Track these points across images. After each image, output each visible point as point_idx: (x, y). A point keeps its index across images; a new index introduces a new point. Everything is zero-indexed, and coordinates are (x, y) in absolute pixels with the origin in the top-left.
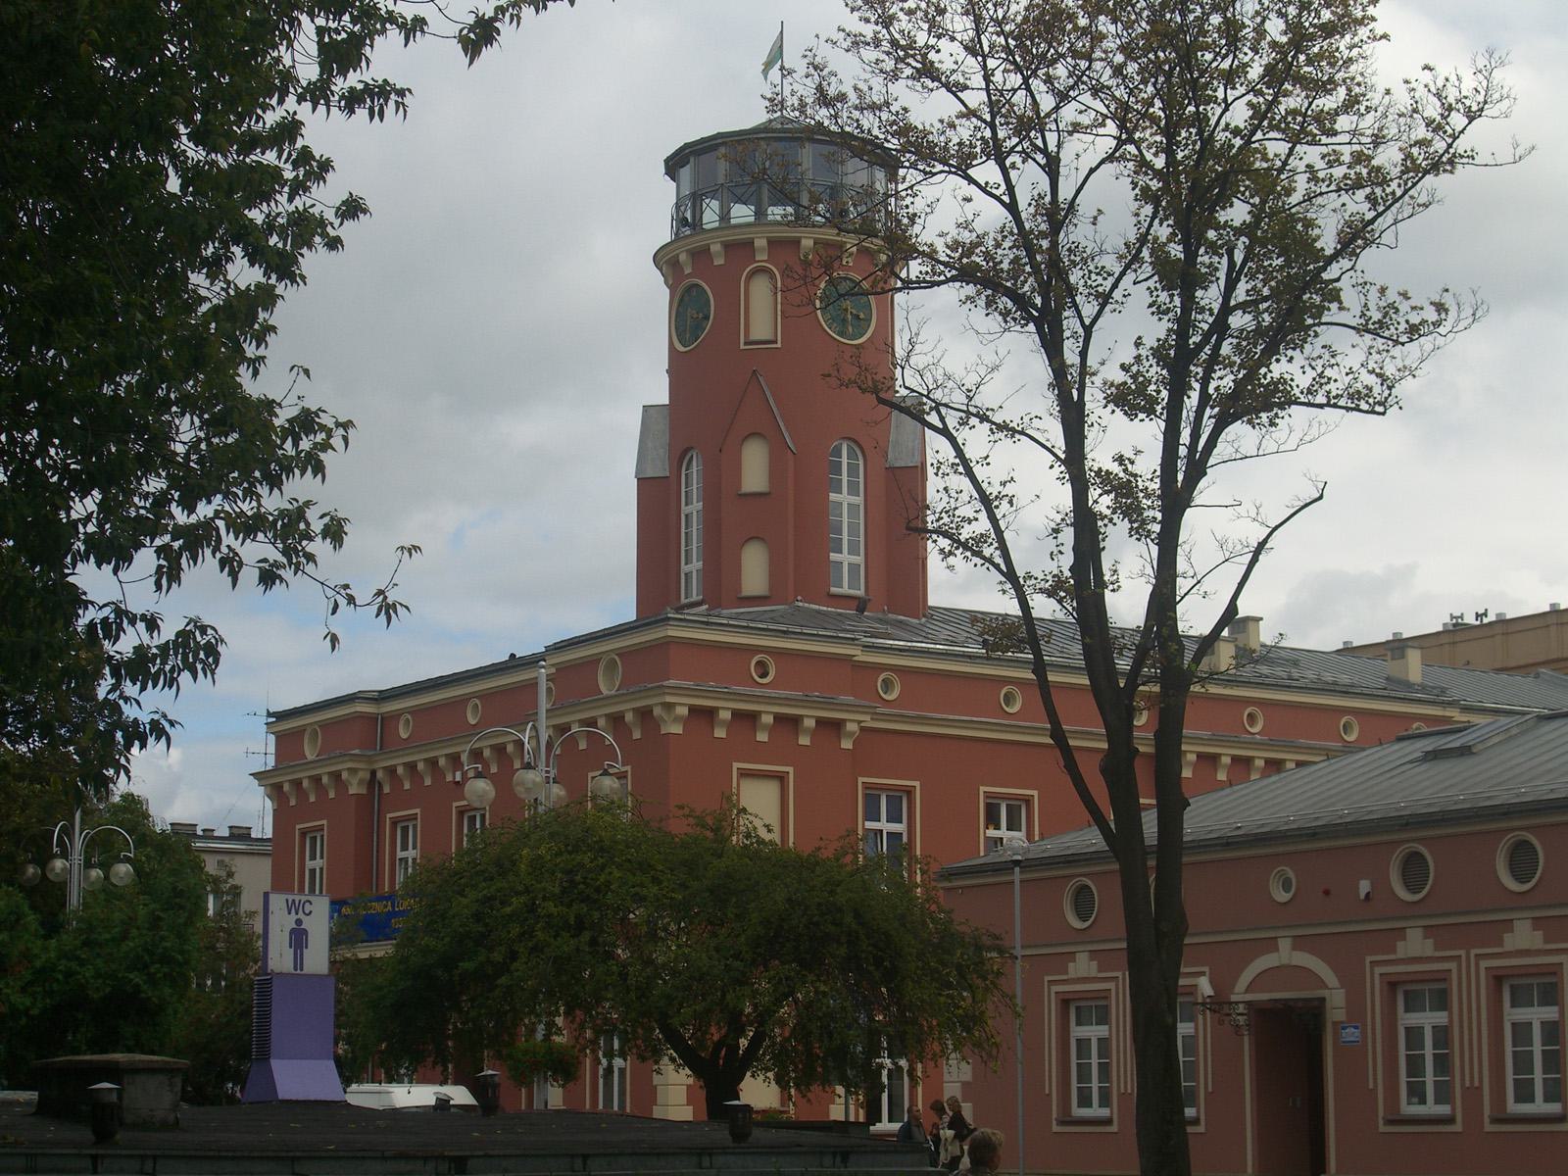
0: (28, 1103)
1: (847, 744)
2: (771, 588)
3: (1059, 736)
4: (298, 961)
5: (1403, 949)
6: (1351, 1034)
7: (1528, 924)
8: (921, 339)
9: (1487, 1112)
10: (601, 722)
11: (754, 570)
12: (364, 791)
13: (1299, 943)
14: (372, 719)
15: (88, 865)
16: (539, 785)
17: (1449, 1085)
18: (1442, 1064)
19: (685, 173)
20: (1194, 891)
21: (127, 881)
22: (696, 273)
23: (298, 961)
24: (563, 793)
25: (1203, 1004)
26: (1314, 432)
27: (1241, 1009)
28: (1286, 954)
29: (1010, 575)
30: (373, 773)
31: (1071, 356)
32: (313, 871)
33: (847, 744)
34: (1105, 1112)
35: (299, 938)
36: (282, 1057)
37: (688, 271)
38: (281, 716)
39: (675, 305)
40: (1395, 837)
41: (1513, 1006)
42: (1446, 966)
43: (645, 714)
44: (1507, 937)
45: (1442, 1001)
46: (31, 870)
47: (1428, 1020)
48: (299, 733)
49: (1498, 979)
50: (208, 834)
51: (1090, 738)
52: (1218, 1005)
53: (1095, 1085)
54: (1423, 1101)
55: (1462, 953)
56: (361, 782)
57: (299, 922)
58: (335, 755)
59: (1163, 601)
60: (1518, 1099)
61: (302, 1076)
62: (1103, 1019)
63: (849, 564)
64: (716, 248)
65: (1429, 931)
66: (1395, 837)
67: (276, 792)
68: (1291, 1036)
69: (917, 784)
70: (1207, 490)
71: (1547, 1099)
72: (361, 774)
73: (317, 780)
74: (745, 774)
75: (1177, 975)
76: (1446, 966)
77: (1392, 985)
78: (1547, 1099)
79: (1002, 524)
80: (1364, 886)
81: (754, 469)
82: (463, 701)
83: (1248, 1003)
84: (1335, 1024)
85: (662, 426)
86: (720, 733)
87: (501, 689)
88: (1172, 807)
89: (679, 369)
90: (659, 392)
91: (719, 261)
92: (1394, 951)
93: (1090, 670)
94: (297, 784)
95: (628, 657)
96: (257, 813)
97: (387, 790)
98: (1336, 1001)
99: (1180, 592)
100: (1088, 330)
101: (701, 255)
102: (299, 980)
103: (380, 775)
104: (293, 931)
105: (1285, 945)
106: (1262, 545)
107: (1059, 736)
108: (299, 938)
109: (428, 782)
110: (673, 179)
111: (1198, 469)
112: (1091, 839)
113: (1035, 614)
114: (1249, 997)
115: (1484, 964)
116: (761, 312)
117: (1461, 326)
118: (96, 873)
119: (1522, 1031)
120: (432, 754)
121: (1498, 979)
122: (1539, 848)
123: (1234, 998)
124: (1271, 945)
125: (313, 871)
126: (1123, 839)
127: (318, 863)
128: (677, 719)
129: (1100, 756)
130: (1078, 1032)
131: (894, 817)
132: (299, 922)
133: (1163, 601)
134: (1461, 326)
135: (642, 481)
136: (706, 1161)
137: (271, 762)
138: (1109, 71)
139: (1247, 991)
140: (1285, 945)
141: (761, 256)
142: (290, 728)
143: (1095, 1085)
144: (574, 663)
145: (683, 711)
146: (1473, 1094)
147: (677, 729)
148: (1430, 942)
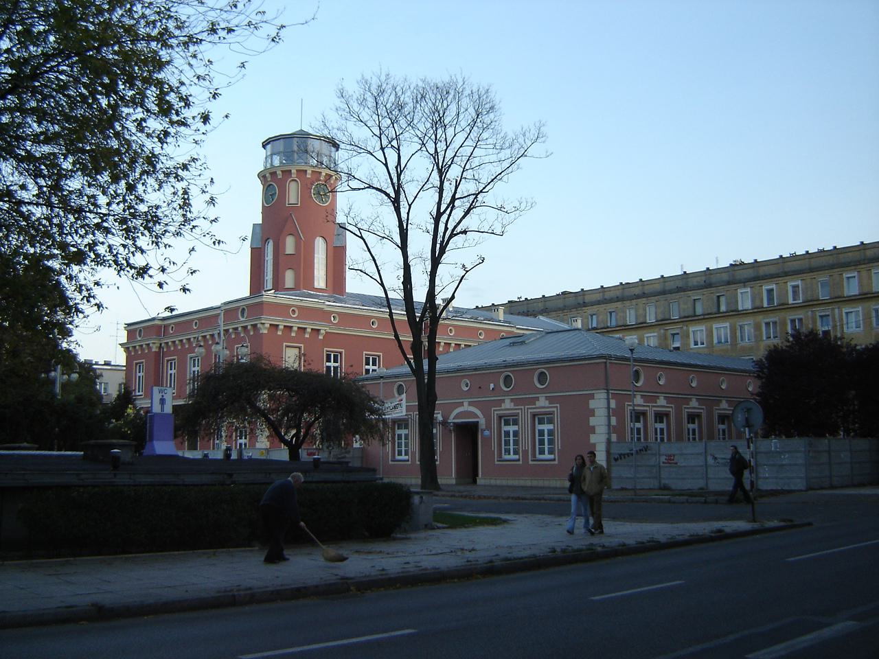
0: (81, 456)
1: (321, 337)
2: (295, 285)
3: (397, 336)
4: (162, 409)
5: (538, 404)
6: (487, 433)
7: (509, 400)
8: (353, 207)
9: (530, 459)
10: (240, 329)
11: (289, 278)
12: (157, 350)
13: (470, 404)
14: (160, 327)
15: (63, 374)
16: (222, 352)
17: (554, 448)
18: (516, 443)
19: (269, 147)
20: (439, 389)
21: (74, 380)
22: (272, 181)
23: (162, 409)
24: (228, 352)
25: (439, 423)
26: (481, 240)
27: (452, 424)
28: (466, 407)
29: (382, 284)
30: (161, 344)
31: (404, 216)
32: (171, 374)
33: (321, 337)
34: (407, 457)
35: (162, 401)
36: (158, 440)
37: (269, 179)
38: (129, 325)
39: (265, 189)
40: (502, 370)
41: (505, 425)
42: (518, 411)
43: (255, 326)
44: (537, 402)
45: (515, 423)
46: (43, 375)
47: (512, 428)
48: (135, 330)
49: (534, 416)
50: (97, 364)
51: (407, 337)
52: (444, 423)
53: (403, 449)
54: (509, 454)
55: (523, 407)
56: (157, 347)
57: (163, 396)
58: (150, 340)
59: (431, 295)
60: (540, 454)
61: (163, 447)
62: (550, 421)
63: (320, 280)
64: (309, 172)
65: (512, 400)
66: (502, 370)
67: (127, 350)
68: (468, 433)
69: (343, 350)
70: (446, 258)
71: (514, 454)
72: (156, 345)
73: (141, 346)
74: (287, 346)
75: (434, 413)
76: (518, 411)
77: (500, 417)
78: (514, 454)
79: (379, 268)
80: (492, 386)
81: (290, 246)
82: (193, 320)
83: (454, 423)
84: (482, 430)
85: (258, 230)
86: (280, 333)
87: (206, 318)
88: (433, 360)
89: (266, 212)
90: (259, 220)
91: (308, 176)
92: (501, 406)
93: (408, 315)
94: (135, 347)
95: (249, 308)
96: (120, 358)
97: (165, 350)
98: (482, 422)
99: (436, 294)
100: (410, 206)
101: (273, 174)
102: (162, 416)
103: (163, 345)
104: (161, 399)
105: (466, 404)
106: (463, 276)
107: (397, 336)
108: (162, 401)
109: (179, 347)
110: (265, 149)
111: (443, 251)
112: (407, 369)
113: (389, 297)
114: (454, 421)
115: (530, 411)
116: (293, 194)
117: (527, 208)
118: (66, 377)
119: (507, 434)
120: (189, 337)
121: (534, 416)
122: (547, 373)
123: (449, 421)
124: (462, 404)
125: (171, 374)
126: (417, 371)
127: (173, 372)
128: (266, 328)
129: (410, 343)
130: (539, 427)
131: (335, 361)
132: (163, 396)
133: (431, 295)
134: (527, 208)
135: (252, 249)
136: (308, 474)
137: (126, 341)
138: (401, 122)
139: (454, 419)
140: (466, 404)
141: (294, 176)
142: (133, 330)
143: (403, 449)
144: (231, 310)
145: (268, 326)
146: (525, 453)
147: (266, 332)
148: (512, 404)
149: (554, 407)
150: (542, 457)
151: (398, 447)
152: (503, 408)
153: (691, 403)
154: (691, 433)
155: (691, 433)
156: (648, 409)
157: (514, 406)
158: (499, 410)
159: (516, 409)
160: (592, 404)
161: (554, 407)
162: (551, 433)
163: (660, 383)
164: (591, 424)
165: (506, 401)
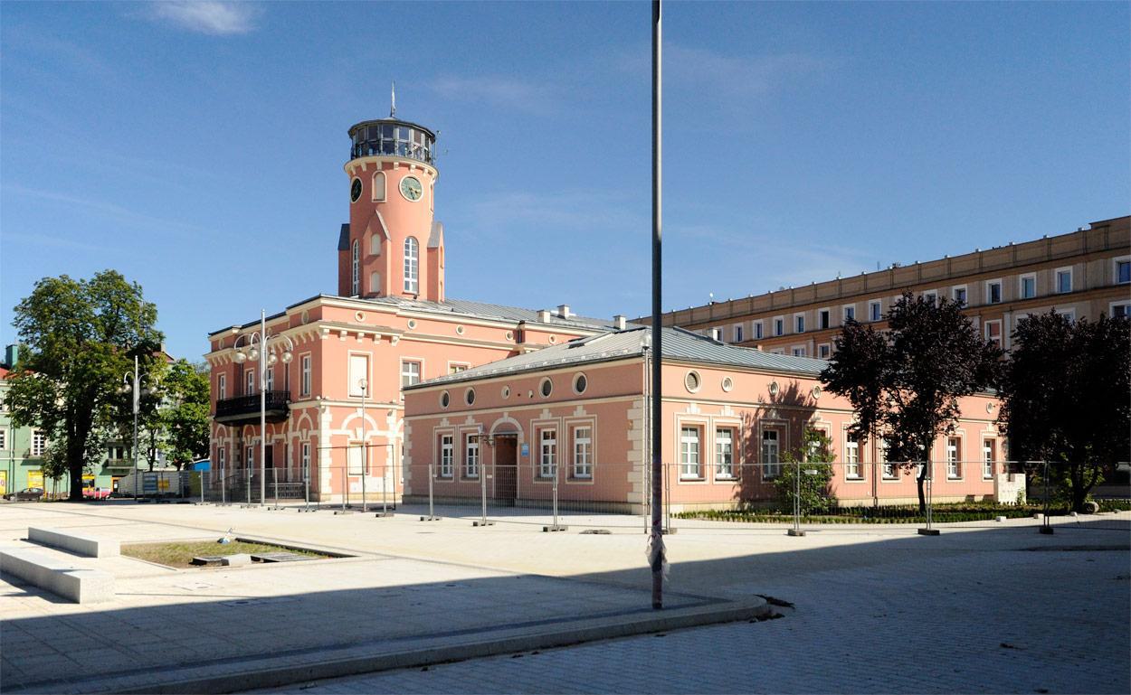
5: (576, 414)
13: (511, 414)
28: (506, 419)
34: (450, 475)
44: (575, 412)
47: (550, 443)
60: (578, 473)
80: (531, 393)
92: (572, 415)
115: (567, 422)
119: (546, 448)
124: (501, 415)
149: (592, 418)
150: (580, 475)
151: (578, 452)
152: (688, 412)
153: (466, 422)
154: (474, 469)
155: (474, 469)
156: (707, 420)
157: (553, 416)
158: (571, 419)
159: (588, 418)
160: (631, 414)
161: (592, 418)
162: (588, 446)
163: (508, 389)
164: (629, 439)
165: (692, 405)
